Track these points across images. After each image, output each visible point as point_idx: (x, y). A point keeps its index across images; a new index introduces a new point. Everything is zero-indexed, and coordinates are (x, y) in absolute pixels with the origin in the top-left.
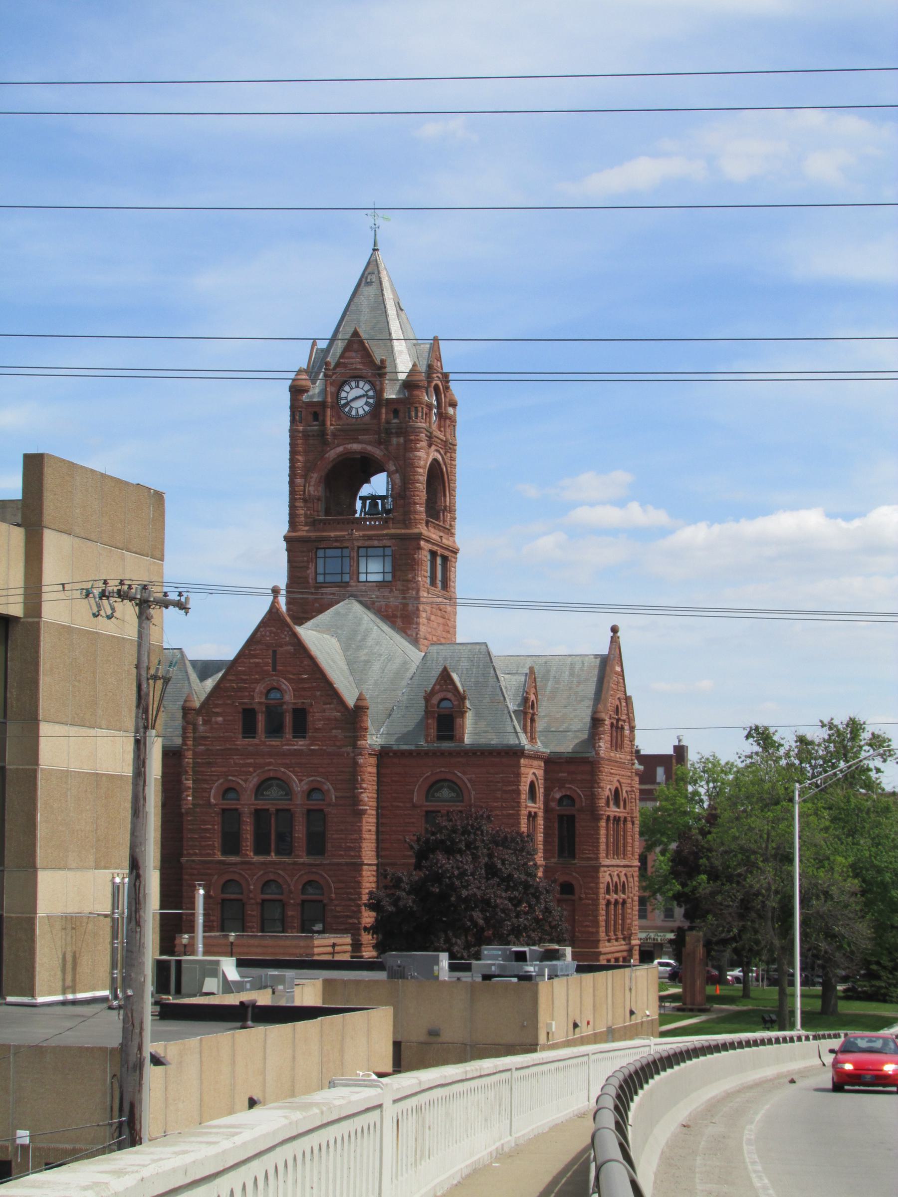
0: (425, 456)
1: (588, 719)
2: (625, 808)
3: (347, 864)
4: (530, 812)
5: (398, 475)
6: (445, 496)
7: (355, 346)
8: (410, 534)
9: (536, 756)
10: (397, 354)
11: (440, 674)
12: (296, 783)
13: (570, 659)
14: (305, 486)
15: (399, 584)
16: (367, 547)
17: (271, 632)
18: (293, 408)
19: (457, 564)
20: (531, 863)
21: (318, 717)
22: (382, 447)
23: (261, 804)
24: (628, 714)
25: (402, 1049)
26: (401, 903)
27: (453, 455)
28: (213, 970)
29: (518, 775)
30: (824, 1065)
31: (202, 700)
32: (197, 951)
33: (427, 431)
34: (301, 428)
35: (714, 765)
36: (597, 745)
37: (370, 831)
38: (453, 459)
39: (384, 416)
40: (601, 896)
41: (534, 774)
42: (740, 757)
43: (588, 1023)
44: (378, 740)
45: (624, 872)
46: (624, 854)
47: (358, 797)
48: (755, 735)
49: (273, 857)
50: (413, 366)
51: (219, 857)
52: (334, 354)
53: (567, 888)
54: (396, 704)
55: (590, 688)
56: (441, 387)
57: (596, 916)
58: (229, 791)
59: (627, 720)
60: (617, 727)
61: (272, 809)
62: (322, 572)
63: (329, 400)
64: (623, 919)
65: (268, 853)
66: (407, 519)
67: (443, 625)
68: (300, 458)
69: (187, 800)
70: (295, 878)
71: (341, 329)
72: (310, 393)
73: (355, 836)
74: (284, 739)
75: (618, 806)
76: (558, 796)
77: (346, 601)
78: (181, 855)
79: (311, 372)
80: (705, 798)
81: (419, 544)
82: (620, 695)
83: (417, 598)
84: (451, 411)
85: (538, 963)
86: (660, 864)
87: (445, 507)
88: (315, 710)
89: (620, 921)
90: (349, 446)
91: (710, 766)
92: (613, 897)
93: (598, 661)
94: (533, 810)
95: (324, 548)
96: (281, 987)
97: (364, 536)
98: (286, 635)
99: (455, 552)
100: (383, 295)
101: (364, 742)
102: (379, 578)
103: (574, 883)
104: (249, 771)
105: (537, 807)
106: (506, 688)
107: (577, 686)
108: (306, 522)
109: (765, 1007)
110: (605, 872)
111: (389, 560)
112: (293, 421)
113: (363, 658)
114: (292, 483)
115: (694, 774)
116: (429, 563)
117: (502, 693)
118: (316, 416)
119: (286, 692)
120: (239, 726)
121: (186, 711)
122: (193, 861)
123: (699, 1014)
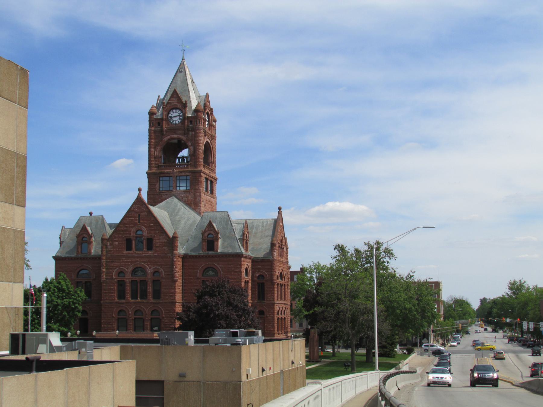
0: (203, 140)
1: (269, 244)
2: (284, 280)
3: (169, 302)
4: (246, 281)
5: (192, 147)
6: (212, 157)
7: (175, 96)
8: (197, 170)
9: (248, 257)
10: (192, 99)
11: (208, 224)
12: (148, 268)
13: (262, 221)
14: (155, 152)
15: (193, 191)
16: (180, 176)
17: (138, 207)
18: (150, 121)
19: (217, 184)
20: (246, 300)
21: (158, 240)
22: (186, 136)
23: (134, 278)
24: (285, 243)
25: (165, 385)
26: (190, 317)
27: (215, 141)
28: (44, 340)
29: (241, 265)
30: (399, 389)
31: (110, 235)
32: (43, 329)
33: (204, 129)
34: (153, 129)
35: (319, 267)
36: (273, 254)
37: (179, 289)
38: (215, 143)
39: (186, 123)
40: (275, 316)
41: (247, 265)
42: (332, 257)
43: (270, 369)
44: (183, 251)
45: (284, 306)
46: (285, 299)
47: (174, 275)
48: (338, 248)
49: (139, 300)
50: (198, 103)
51: (117, 300)
52: (166, 99)
53: (261, 313)
54: (190, 236)
55: (270, 232)
56: (209, 112)
57: (274, 324)
58: (120, 273)
59: (285, 245)
60: (281, 248)
61: (139, 280)
62: (162, 186)
63: (164, 117)
64: (284, 325)
65: (137, 298)
66: (196, 165)
67: (211, 208)
68: (153, 141)
69: (103, 277)
70: (148, 309)
71: (169, 90)
72: (157, 115)
73: (172, 291)
74: (143, 251)
75: (282, 280)
76: (257, 275)
77: (171, 198)
78: (101, 300)
79: (158, 107)
80: (315, 279)
81: (201, 174)
82: (282, 235)
83: (200, 196)
84: (214, 123)
85: (244, 337)
86: (298, 305)
87: (212, 161)
88: (156, 239)
89: (283, 326)
90: (172, 136)
91: (317, 266)
92: (280, 316)
93: (273, 221)
94: (247, 280)
95: (163, 177)
96: (84, 350)
97: (178, 171)
98: (144, 208)
99: (216, 179)
100: (186, 76)
101: (176, 252)
102: (185, 188)
103: (264, 310)
104: (129, 265)
105: (249, 278)
106: (235, 229)
107: (265, 231)
108: (155, 166)
109: (342, 360)
110: (277, 306)
111: (188, 181)
112: (150, 126)
113: (177, 219)
114: (149, 151)
115: (311, 270)
116: (205, 183)
117: (234, 231)
118: (159, 124)
119: (144, 231)
120: (124, 246)
121: (103, 240)
122: (106, 302)
123: (316, 363)
